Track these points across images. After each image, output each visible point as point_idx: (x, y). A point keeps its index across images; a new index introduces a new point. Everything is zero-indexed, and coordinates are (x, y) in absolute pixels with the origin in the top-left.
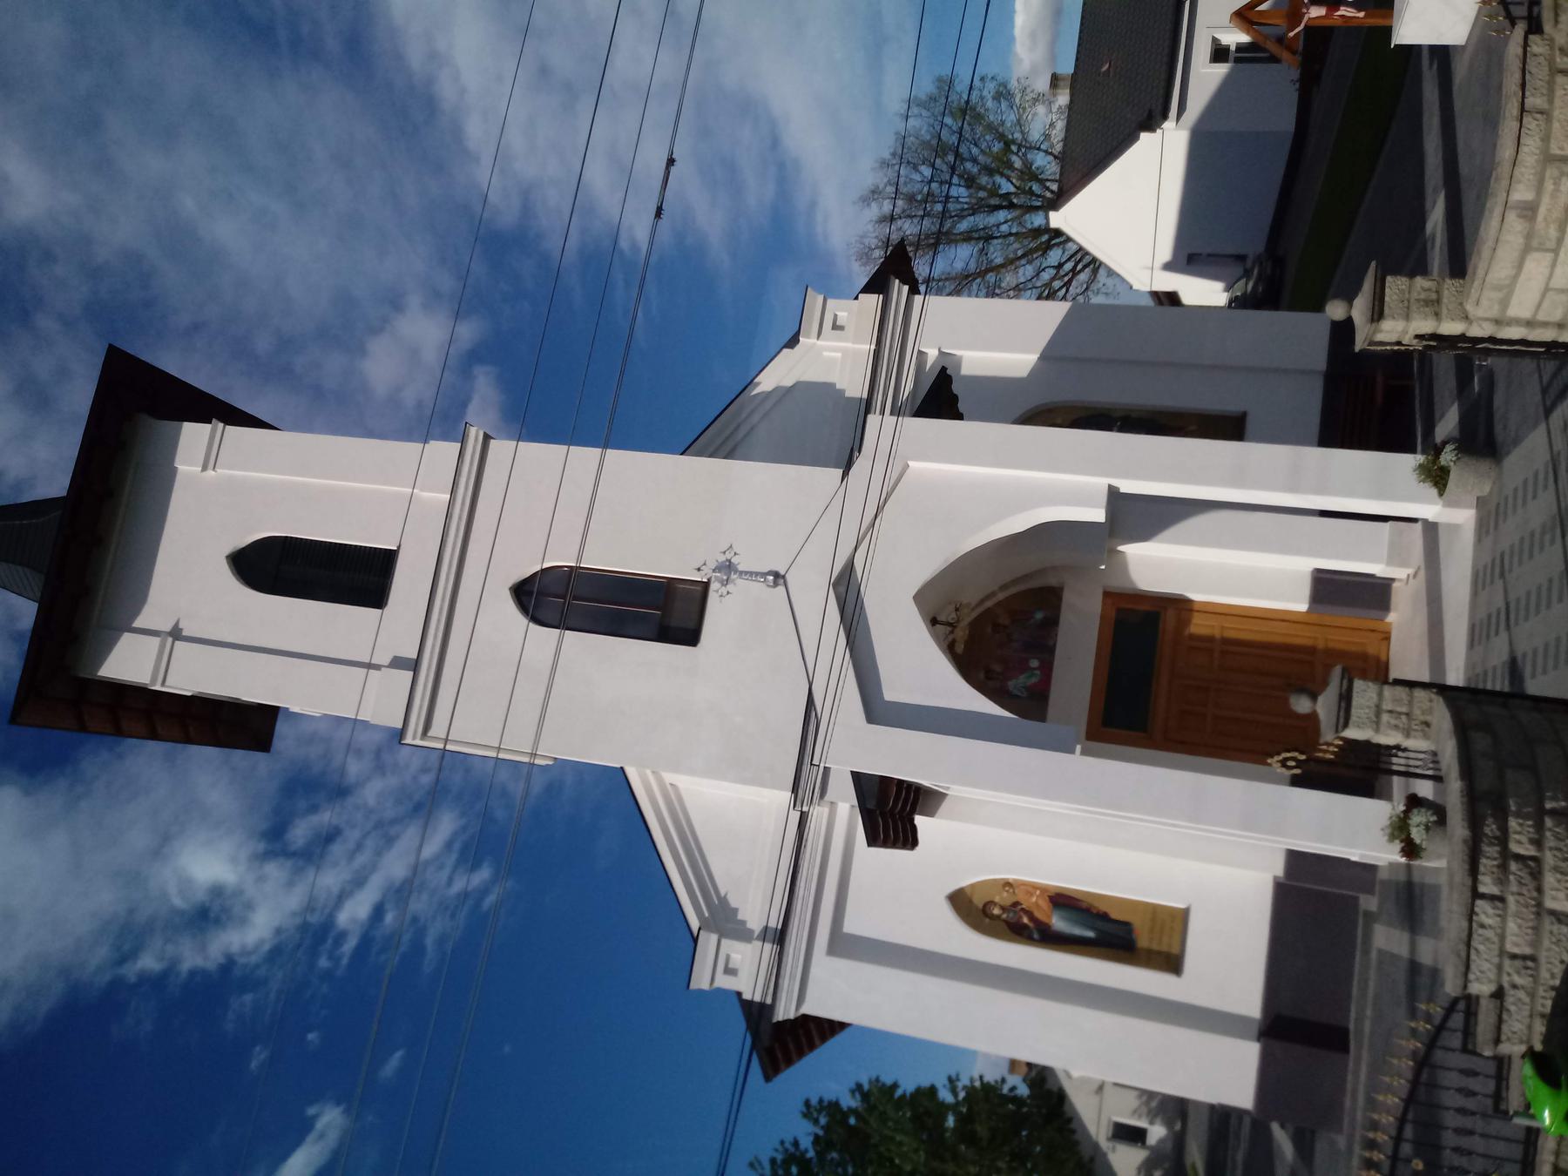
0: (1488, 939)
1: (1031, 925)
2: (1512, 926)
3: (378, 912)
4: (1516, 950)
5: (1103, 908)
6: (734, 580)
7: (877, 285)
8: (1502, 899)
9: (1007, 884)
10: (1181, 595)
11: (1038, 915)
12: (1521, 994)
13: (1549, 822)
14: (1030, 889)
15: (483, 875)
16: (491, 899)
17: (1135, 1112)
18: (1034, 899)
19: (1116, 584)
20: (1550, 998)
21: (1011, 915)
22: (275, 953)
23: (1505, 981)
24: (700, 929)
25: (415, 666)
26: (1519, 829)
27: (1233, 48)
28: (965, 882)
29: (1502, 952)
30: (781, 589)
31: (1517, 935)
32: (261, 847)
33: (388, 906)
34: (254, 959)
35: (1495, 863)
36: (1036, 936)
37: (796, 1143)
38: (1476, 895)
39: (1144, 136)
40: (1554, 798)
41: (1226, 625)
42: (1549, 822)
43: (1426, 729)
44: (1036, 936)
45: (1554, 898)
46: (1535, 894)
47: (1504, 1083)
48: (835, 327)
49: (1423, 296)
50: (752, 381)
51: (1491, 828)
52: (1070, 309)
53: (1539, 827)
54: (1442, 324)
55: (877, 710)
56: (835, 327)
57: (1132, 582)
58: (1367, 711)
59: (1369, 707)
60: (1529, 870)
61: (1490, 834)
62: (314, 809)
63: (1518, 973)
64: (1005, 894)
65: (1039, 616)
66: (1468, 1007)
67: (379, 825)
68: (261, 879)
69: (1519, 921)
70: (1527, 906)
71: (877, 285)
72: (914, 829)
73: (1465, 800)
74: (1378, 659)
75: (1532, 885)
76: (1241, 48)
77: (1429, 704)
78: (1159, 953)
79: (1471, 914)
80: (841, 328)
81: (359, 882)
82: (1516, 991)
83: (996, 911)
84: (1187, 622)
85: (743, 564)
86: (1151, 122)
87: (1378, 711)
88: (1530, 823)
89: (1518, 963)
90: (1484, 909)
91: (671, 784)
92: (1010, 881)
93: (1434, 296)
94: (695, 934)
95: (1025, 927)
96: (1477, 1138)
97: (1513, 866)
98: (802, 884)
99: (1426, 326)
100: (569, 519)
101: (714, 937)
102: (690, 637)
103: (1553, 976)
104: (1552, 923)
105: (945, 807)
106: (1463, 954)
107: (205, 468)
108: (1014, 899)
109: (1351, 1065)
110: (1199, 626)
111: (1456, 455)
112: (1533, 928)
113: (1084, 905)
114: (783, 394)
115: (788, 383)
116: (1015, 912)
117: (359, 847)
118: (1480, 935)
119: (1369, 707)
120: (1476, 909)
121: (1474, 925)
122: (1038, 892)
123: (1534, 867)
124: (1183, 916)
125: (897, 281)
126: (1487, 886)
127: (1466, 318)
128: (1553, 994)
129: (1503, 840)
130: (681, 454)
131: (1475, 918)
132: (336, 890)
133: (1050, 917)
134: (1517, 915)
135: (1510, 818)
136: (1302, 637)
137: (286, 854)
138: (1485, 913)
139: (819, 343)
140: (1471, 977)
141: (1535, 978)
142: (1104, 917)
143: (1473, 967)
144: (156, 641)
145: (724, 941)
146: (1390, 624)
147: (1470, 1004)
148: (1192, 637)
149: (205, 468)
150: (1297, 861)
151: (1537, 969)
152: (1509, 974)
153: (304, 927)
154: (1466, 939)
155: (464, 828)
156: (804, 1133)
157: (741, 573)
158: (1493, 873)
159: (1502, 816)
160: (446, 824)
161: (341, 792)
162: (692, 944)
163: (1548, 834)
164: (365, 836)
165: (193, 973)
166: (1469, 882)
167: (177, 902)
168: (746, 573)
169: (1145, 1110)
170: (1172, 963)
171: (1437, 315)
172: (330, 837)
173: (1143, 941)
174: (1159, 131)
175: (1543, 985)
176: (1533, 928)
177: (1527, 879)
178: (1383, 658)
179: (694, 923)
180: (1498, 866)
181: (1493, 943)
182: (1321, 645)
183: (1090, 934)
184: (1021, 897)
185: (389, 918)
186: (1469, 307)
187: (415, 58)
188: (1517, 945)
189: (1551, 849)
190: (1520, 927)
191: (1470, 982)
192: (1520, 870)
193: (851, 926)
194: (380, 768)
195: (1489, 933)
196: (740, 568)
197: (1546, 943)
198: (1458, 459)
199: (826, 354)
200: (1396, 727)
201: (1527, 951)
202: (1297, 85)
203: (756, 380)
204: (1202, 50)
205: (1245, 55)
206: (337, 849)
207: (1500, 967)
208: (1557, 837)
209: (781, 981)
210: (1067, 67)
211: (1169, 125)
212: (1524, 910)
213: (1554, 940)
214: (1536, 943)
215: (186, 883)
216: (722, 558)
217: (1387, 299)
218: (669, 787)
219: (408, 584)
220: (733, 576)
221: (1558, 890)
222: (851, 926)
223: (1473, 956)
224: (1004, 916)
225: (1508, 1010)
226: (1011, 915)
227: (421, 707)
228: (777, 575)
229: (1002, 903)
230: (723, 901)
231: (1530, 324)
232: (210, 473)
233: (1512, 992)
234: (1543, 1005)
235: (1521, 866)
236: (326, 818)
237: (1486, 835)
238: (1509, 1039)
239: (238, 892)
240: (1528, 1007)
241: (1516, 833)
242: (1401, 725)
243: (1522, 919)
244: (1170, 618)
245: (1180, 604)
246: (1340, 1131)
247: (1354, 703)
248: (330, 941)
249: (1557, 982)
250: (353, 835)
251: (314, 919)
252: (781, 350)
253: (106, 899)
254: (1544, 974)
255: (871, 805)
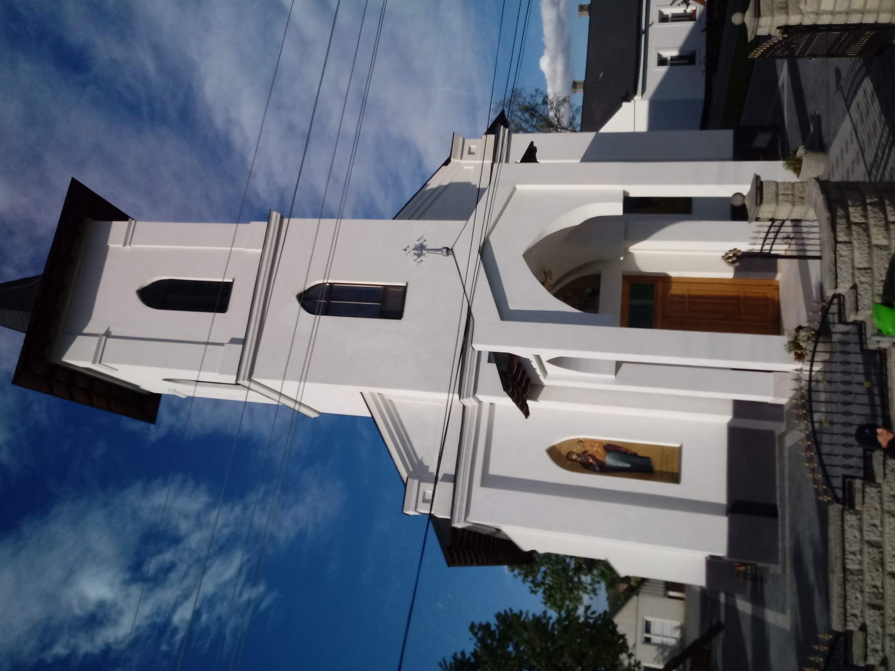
0: (845, 262)
1: (594, 463)
2: (857, 254)
3: (197, 614)
4: (860, 266)
5: (634, 450)
6: (424, 254)
7: (493, 130)
8: (850, 243)
9: (580, 441)
10: (665, 274)
11: (597, 457)
12: (866, 286)
13: (869, 207)
14: (593, 443)
15: (261, 588)
16: (265, 604)
17: (655, 659)
18: (595, 449)
19: (629, 269)
20: (882, 286)
21: (583, 458)
22: (135, 642)
23: (857, 280)
24: (408, 478)
25: (244, 342)
26: (854, 211)
27: (669, 59)
28: (556, 442)
29: (853, 267)
30: (451, 257)
31: (860, 258)
32: (128, 576)
33: (203, 610)
34: (122, 646)
35: (845, 226)
36: (597, 469)
37: (463, 654)
38: (836, 242)
39: (625, 104)
40: (870, 198)
41: (690, 288)
42: (869, 207)
43: (802, 200)
44: (597, 469)
45: (877, 239)
46: (867, 238)
47: (863, 336)
48: (470, 153)
49: (779, 6)
50: (426, 184)
51: (840, 212)
52: (595, 137)
53: (865, 209)
54: (790, 17)
55: (505, 313)
56: (470, 153)
57: (638, 268)
58: (771, 195)
59: (772, 193)
60: (862, 228)
61: (840, 215)
62: (160, 552)
63: (863, 276)
64: (579, 447)
65: (589, 290)
66: (839, 301)
67: (198, 560)
68: (127, 596)
69: (860, 251)
70: (863, 244)
71: (493, 130)
72: (527, 406)
73: (826, 201)
74: (773, 300)
75: (864, 234)
76: (673, 59)
77: (802, 188)
78: (667, 473)
79: (835, 251)
80: (473, 154)
81: (186, 596)
82: (863, 285)
83: (574, 457)
84: (669, 288)
85: (429, 245)
86: (628, 97)
87: (777, 195)
88: (860, 208)
89: (862, 272)
90: (843, 250)
91: (389, 400)
92: (582, 440)
93: (785, 5)
94: (405, 480)
95: (591, 464)
96: (854, 417)
97: (854, 227)
98: (467, 431)
99: (781, 20)
100: (317, 319)
101: (416, 482)
102: (397, 314)
103: (881, 275)
104: (877, 250)
105: (544, 392)
106: (833, 269)
107: (125, 244)
108: (583, 450)
109: (780, 523)
110: (675, 290)
111: (805, 151)
112: (868, 254)
113: (623, 450)
114: (443, 189)
115: (446, 183)
116: (585, 457)
117: (186, 574)
118: (841, 261)
119: (772, 193)
120: (837, 249)
121: (837, 256)
122: (597, 445)
123: (865, 227)
124: (678, 452)
125: (502, 127)
126: (842, 237)
127: (801, 13)
128: (882, 284)
129: (847, 216)
130: (394, 219)
131: (837, 253)
132: (172, 602)
133: (604, 458)
134: (859, 248)
135: (849, 208)
136: (732, 292)
137: (144, 579)
138: (842, 250)
139: (462, 162)
140: (839, 281)
141: (872, 277)
142: (635, 455)
143: (839, 276)
144: (96, 339)
145: (422, 484)
146: (778, 281)
147: (847, 636)
148: (673, 296)
149: (125, 244)
150: (741, 408)
151: (872, 273)
152: (858, 277)
153: (153, 626)
154: (834, 262)
155: (249, 560)
156: (469, 645)
157: (428, 250)
158: (844, 231)
159: (846, 208)
160: (237, 559)
161: (175, 540)
162: (403, 487)
163: (869, 212)
164: (190, 567)
165: (86, 656)
166: (832, 235)
167: (78, 612)
168: (431, 250)
169: (661, 658)
170: (674, 477)
171: (787, 13)
172: (169, 568)
173: (657, 467)
174: (632, 101)
175: (876, 280)
176: (868, 254)
177: (862, 232)
178: (776, 299)
179: (404, 474)
180: (846, 228)
181: (849, 263)
182: (742, 295)
183: (628, 465)
184: (588, 448)
185: (204, 618)
186: (802, 6)
187: (219, 121)
188: (860, 263)
189: (872, 218)
190: (861, 254)
191: (839, 283)
192: (857, 229)
193: (493, 470)
194: (199, 525)
195: (846, 259)
196: (428, 247)
197: (875, 260)
198: (806, 153)
199: (465, 167)
200: (787, 201)
201: (866, 265)
202: (705, 74)
203: (428, 183)
204: (652, 60)
205: (675, 62)
206: (173, 576)
207: (853, 274)
208: (874, 212)
209: (455, 502)
210: (581, 77)
211: (637, 98)
212: (863, 246)
213: (879, 258)
214: (870, 261)
215: (83, 600)
216: (418, 243)
217: (761, 8)
218: (388, 402)
219: (239, 300)
220: (424, 252)
221: (878, 234)
222: (493, 470)
223: (838, 270)
224: (579, 459)
225: (860, 295)
226: (583, 458)
227: (252, 340)
228: (448, 249)
229: (578, 452)
230: (421, 463)
231: (832, 13)
232: (128, 247)
233: (861, 286)
234: (878, 290)
235: (858, 227)
236: (168, 556)
237: (838, 215)
238: (863, 309)
239: (114, 605)
240: (870, 292)
241: (853, 213)
242: (789, 200)
243: (862, 250)
244: (660, 287)
245: (664, 279)
246: (777, 563)
247: (764, 192)
248: (168, 633)
249: (884, 278)
250: (182, 567)
251: (159, 620)
252: (442, 166)
253: (36, 611)
254: (877, 275)
255: (505, 369)
